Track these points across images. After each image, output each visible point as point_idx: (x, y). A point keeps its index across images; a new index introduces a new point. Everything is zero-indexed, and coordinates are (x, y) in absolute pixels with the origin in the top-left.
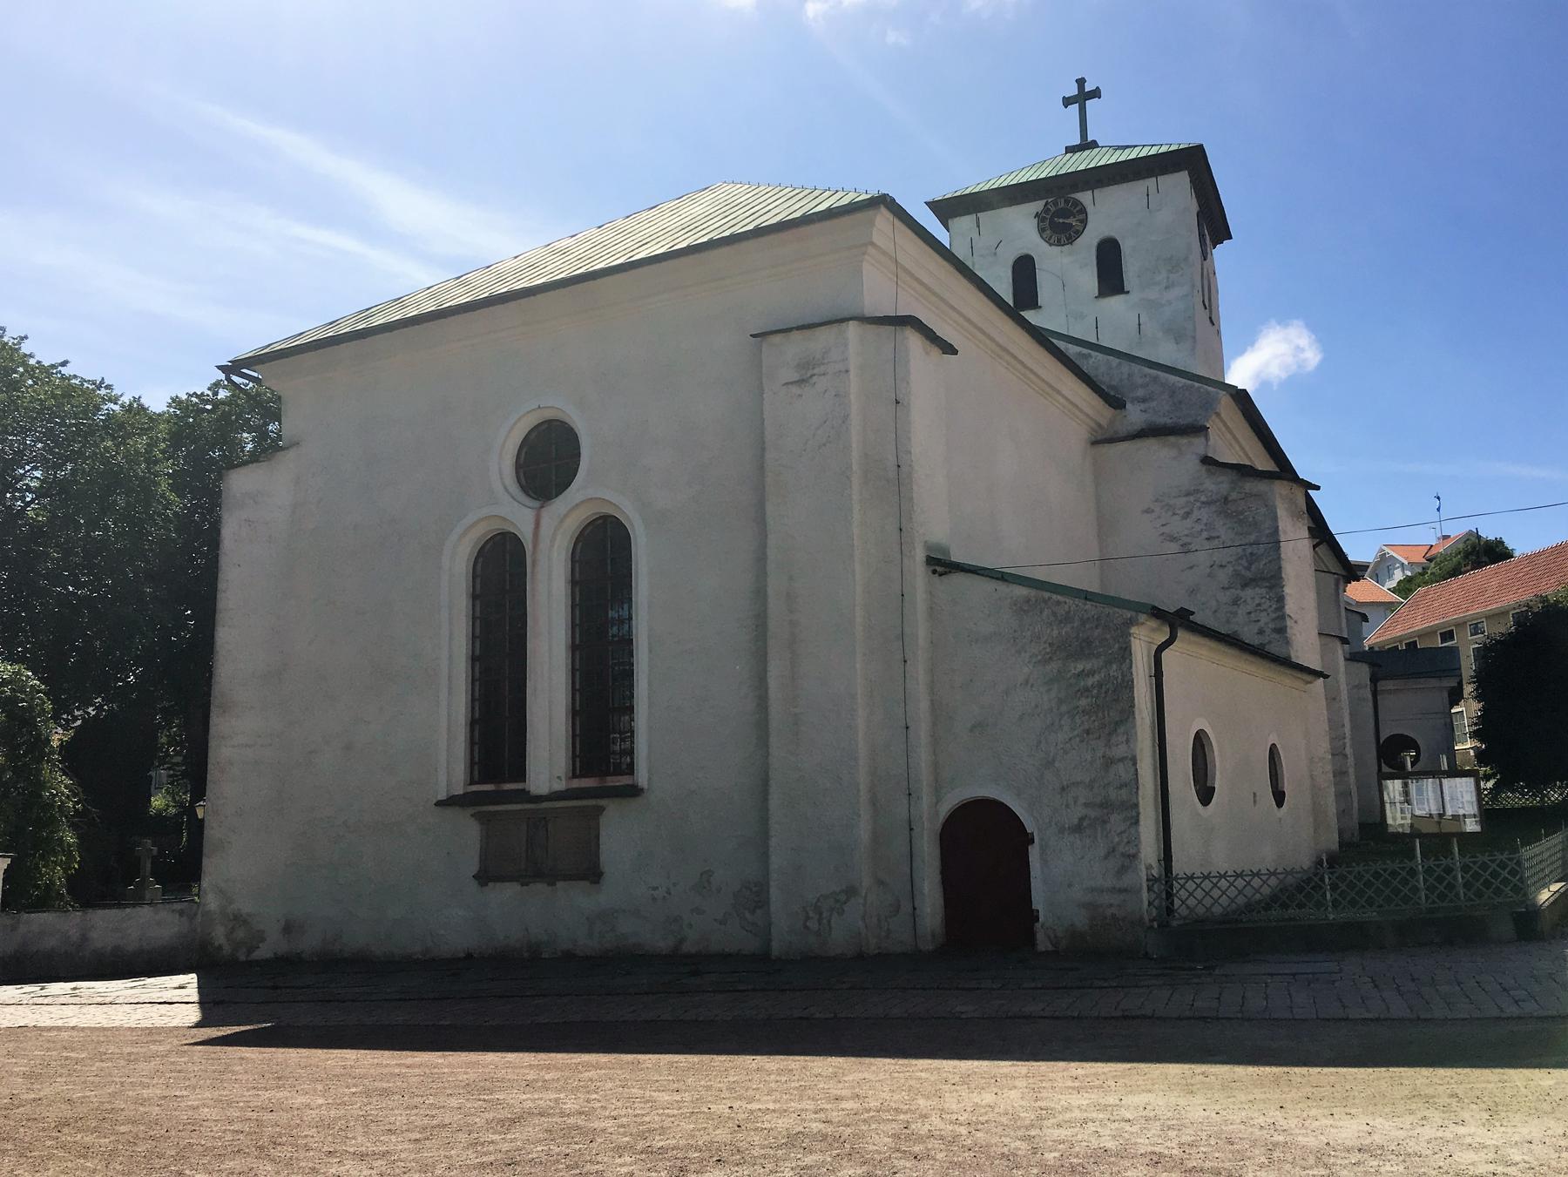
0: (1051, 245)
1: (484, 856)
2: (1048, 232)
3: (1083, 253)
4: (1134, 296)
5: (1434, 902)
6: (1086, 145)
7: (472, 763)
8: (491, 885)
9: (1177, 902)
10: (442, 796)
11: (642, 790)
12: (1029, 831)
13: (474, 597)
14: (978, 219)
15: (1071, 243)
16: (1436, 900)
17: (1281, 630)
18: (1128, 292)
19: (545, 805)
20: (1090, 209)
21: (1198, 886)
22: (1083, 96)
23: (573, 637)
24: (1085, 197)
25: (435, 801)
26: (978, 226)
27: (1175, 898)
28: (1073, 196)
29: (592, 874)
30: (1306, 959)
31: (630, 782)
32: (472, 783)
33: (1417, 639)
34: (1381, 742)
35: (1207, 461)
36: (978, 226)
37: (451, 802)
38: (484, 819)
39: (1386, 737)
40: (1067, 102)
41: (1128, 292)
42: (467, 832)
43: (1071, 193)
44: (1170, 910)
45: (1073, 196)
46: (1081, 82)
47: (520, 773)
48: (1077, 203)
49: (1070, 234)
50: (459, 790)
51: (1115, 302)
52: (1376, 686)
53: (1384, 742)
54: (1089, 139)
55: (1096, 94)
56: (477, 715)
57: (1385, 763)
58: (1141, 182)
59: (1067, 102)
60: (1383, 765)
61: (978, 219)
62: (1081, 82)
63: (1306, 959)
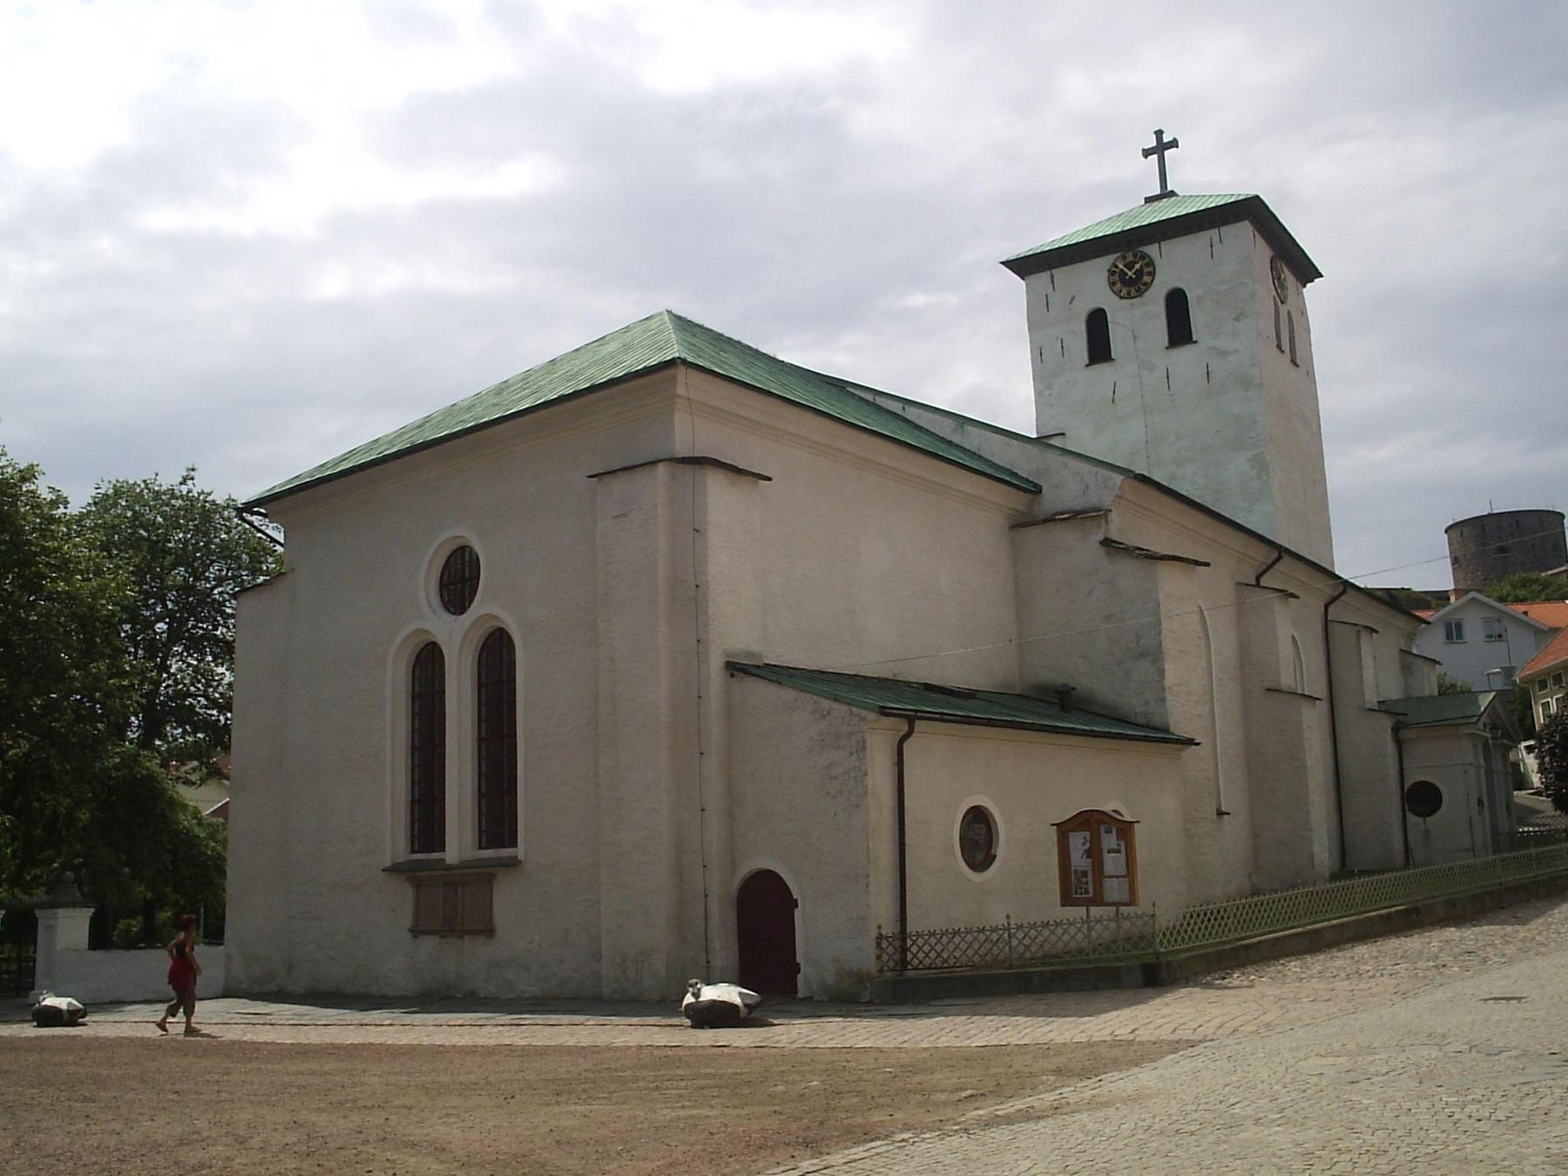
0: (1121, 298)
1: (417, 917)
2: (1119, 285)
3: (1153, 307)
4: (1201, 346)
5: (1100, 954)
6: (1166, 194)
7: (480, 831)
8: (421, 937)
9: (909, 956)
10: (388, 864)
11: (520, 862)
12: (795, 897)
13: (414, 697)
14: (1052, 277)
15: (1140, 296)
16: (1103, 952)
17: (1162, 700)
18: (1196, 342)
19: (455, 872)
20: (1157, 260)
21: (963, 939)
22: (1161, 147)
23: (479, 732)
24: (1152, 250)
25: (382, 868)
26: (1053, 282)
27: (908, 953)
28: (1140, 249)
29: (489, 931)
30: (964, 1003)
31: (513, 854)
32: (413, 852)
33: (1561, 671)
34: (1406, 788)
35: (1107, 543)
36: (1053, 282)
37: (394, 869)
38: (417, 884)
39: (1410, 785)
40: (1147, 153)
41: (1196, 342)
42: (404, 895)
43: (1139, 247)
44: (904, 963)
45: (1140, 249)
46: (1159, 133)
47: (441, 847)
48: (1144, 256)
49: (1139, 287)
50: (401, 859)
51: (1184, 353)
52: (1397, 735)
53: (1409, 790)
54: (1169, 189)
55: (1174, 144)
56: (416, 797)
57: (1410, 810)
58: (1202, 234)
59: (1147, 153)
60: (1407, 813)
61: (1052, 277)
62: (1159, 133)
63: (964, 1003)
